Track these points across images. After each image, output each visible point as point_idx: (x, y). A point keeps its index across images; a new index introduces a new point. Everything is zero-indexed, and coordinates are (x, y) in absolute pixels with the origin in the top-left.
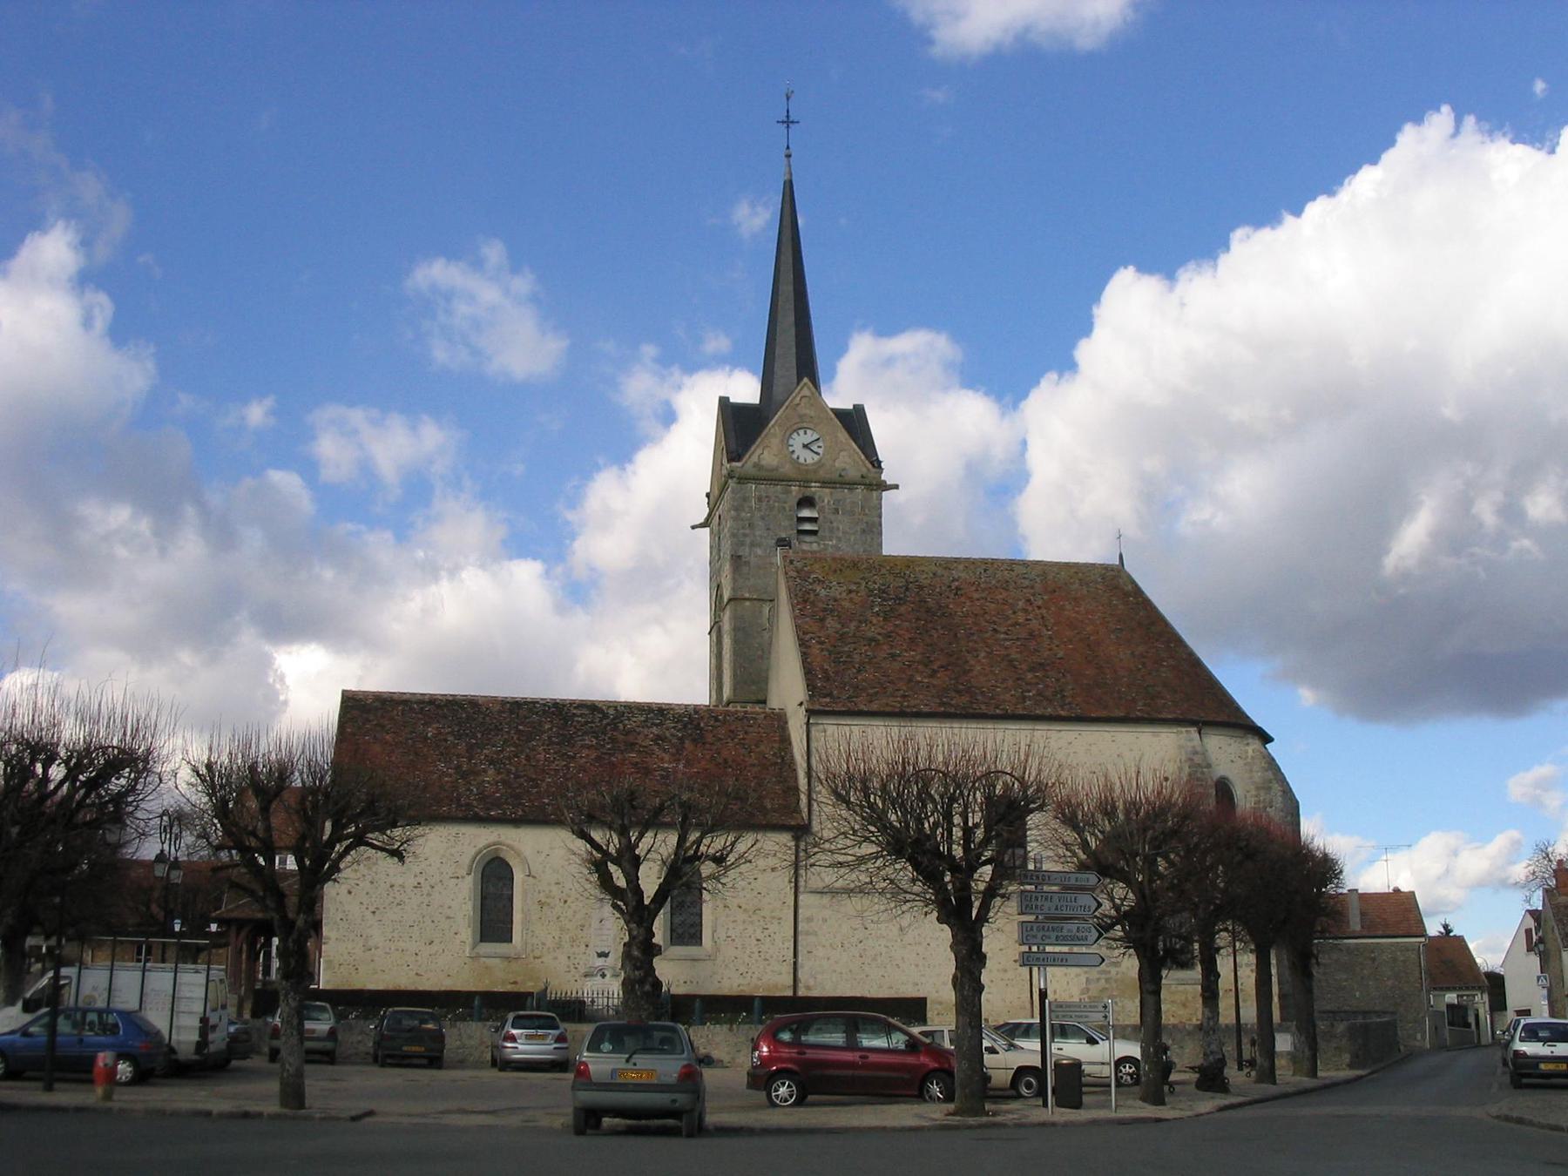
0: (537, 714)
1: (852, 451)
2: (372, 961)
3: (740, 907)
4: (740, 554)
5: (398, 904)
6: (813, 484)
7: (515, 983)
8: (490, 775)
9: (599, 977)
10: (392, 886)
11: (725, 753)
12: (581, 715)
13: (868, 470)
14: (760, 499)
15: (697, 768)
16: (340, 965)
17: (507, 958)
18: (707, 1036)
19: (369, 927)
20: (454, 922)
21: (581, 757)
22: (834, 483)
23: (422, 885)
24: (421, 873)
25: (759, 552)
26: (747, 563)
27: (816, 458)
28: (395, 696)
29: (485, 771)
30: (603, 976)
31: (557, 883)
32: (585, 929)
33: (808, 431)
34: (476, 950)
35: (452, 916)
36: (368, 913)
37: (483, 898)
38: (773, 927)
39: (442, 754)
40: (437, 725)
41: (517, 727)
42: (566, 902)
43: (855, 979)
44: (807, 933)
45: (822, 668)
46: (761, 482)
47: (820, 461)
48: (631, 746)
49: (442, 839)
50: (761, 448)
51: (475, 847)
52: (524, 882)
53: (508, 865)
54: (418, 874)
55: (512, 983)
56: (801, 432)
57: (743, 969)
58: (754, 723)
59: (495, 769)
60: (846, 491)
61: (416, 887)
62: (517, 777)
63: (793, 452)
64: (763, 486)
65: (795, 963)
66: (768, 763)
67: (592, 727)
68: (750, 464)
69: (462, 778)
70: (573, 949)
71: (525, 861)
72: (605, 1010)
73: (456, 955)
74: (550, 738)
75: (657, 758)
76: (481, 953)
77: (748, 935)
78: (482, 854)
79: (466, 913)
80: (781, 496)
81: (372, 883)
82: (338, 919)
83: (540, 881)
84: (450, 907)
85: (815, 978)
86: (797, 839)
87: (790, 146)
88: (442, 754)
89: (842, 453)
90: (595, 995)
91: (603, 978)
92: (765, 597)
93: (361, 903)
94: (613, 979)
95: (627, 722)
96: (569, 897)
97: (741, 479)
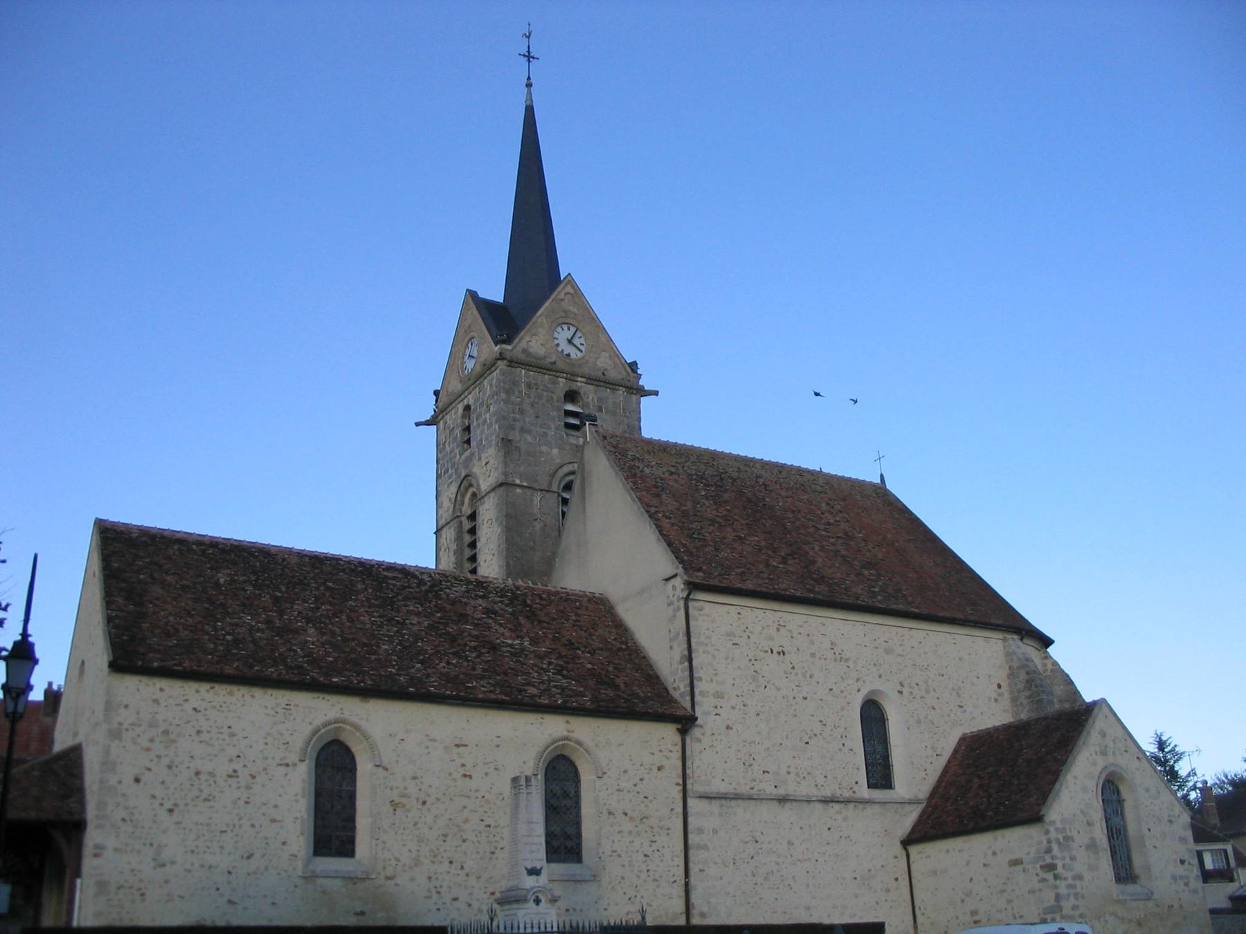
0: (343, 570)
1: (612, 354)
3: (626, 814)
5: (206, 800)
6: (579, 379)
7: (362, 913)
8: (311, 635)
12: (394, 578)
14: (529, 386)
16: (119, 888)
17: (351, 879)
24: (239, 756)
25: (529, 439)
26: (517, 448)
27: (579, 355)
28: (165, 533)
30: (537, 901)
31: (414, 778)
35: (279, 818)
36: (163, 814)
37: (318, 794)
40: (229, 571)
43: (749, 903)
44: (699, 847)
46: (531, 368)
47: (583, 358)
51: (311, 723)
54: (234, 758)
56: (565, 327)
57: (632, 893)
60: (608, 390)
61: (230, 776)
64: (531, 373)
65: (687, 884)
68: (519, 349)
71: (373, 747)
80: (549, 386)
81: (170, 767)
83: (393, 774)
85: (709, 902)
86: (683, 732)
87: (531, 77)
91: (538, 904)
96: (429, 796)
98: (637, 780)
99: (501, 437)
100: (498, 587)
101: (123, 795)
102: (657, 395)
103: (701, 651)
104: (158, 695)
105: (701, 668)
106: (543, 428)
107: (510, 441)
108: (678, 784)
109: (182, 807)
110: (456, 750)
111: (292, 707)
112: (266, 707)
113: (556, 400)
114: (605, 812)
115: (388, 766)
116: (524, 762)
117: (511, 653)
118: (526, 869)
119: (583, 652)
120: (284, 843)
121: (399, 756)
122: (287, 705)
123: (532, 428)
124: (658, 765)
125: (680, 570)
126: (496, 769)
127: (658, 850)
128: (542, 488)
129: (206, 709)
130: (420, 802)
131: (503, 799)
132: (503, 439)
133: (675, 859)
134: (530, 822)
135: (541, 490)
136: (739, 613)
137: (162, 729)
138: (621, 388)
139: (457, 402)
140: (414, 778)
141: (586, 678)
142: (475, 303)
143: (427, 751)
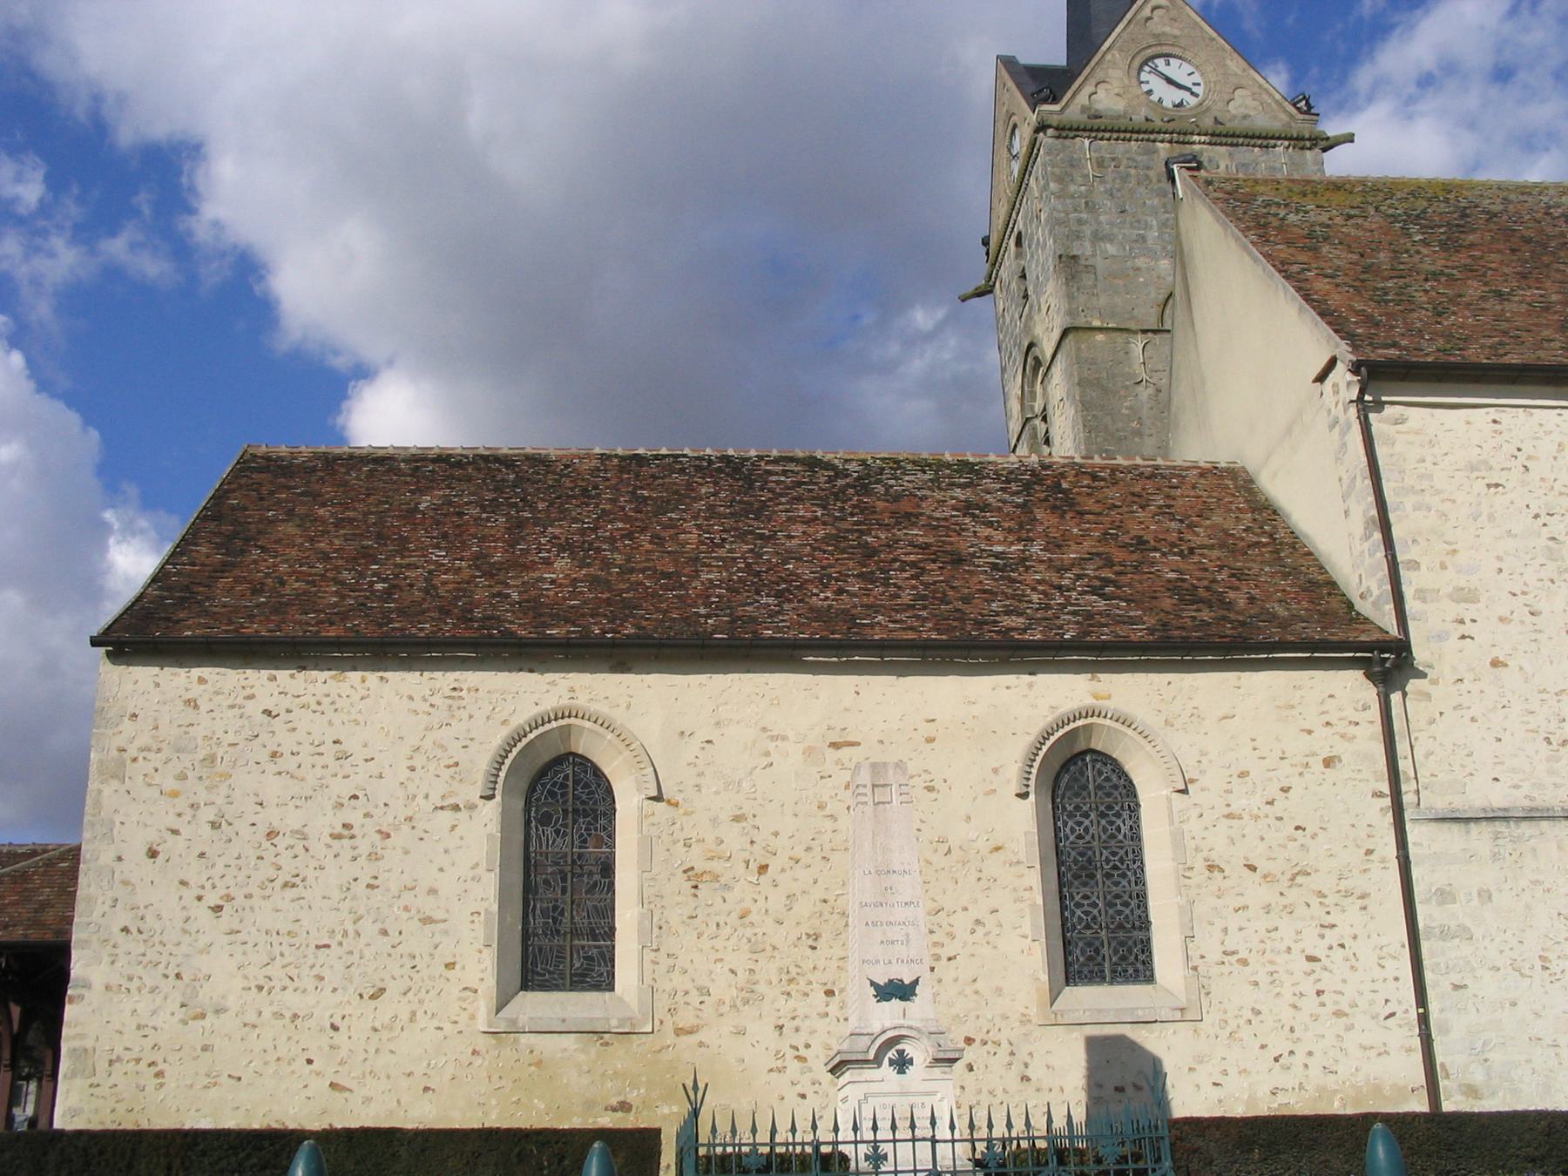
1: (1256, 89)
2: (205, 1048)
3: (1253, 868)
4: (1075, 252)
6: (1196, 138)
7: (624, 1107)
9: (886, 1070)
10: (271, 835)
11: (1135, 529)
13: (1291, 116)
14: (1100, 164)
19: (201, 952)
20: (446, 932)
21: (790, 537)
22: (1233, 136)
24: (355, 797)
26: (1090, 269)
27: (1193, 101)
29: (548, 562)
31: (737, 819)
32: (820, 944)
33: (1171, 60)
34: (507, 1012)
36: (202, 913)
37: (529, 865)
38: (1349, 919)
39: (445, 536)
42: (763, 869)
48: (910, 518)
49: (413, 705)
50: (1093, 81)
51: (505, 722)
52: (643, 816)
53: (598, 773)
55: (614, 1110)
57: (1279, 1045)
60: (1256, 150)
61: (338, 837)
63: (1150, 92)
65: (1424, 1020)
69: (488, 575)
70: (792, 1003)
73: (447, 1027)
74: (711, 508)
76: (523, 1021)
78: (525, 741)
79: (481, 907)
80: (1139, 158)
81: (215, 825)
82: (116, 929)
84: (433, 891)
88: (445, 536)
89: (1238, 92)
90: (884, 1133)
91: (901, 1071)
92: (1132, 325)
93: (183, 883)
94: (937, 1072)
95: (892, 482)
97: (1063, 129)
98: (1273, 792)
99: (1059, 253)
100: (1004, 469)
101: (126, 883)
102: (1352, 141)
103: (1408, 507)
104: (196, 691)
105: (1414, 541)
106: (1134, 228)
107: (1074, 257)
108: (1380, 795)
109: (240, 900)
110: (832, 754)
111: (463, 694)
112: (411, 698)
113: (1154, 180)
114: (1200, 865)
115: (679, 798)
116: (995, 771)
117: (994, 567)
118: (873, 984)
119: (1164, 554)
120: (450, 966)
121: (700, 775)
122: (455, 689)
123: (1115, 230)
124: (1326, 754)
125: (1343, 350)
126: (930, 789)
127: (1342, 946)
128: (1146, 327)
129: (289, 711)
130: (754, 866)
131: (949, 851)
132: (1060, 256)
133: (1388, 963)
134: (884, 872)
135: (1144, 332)
136: (1495, 422)
137: (201, 754)
138: (1279, 143)
139: (1007, 237)
140: (737, 819)
141: (1158, 595)
142: (1010, 73)
143: (765, 761)
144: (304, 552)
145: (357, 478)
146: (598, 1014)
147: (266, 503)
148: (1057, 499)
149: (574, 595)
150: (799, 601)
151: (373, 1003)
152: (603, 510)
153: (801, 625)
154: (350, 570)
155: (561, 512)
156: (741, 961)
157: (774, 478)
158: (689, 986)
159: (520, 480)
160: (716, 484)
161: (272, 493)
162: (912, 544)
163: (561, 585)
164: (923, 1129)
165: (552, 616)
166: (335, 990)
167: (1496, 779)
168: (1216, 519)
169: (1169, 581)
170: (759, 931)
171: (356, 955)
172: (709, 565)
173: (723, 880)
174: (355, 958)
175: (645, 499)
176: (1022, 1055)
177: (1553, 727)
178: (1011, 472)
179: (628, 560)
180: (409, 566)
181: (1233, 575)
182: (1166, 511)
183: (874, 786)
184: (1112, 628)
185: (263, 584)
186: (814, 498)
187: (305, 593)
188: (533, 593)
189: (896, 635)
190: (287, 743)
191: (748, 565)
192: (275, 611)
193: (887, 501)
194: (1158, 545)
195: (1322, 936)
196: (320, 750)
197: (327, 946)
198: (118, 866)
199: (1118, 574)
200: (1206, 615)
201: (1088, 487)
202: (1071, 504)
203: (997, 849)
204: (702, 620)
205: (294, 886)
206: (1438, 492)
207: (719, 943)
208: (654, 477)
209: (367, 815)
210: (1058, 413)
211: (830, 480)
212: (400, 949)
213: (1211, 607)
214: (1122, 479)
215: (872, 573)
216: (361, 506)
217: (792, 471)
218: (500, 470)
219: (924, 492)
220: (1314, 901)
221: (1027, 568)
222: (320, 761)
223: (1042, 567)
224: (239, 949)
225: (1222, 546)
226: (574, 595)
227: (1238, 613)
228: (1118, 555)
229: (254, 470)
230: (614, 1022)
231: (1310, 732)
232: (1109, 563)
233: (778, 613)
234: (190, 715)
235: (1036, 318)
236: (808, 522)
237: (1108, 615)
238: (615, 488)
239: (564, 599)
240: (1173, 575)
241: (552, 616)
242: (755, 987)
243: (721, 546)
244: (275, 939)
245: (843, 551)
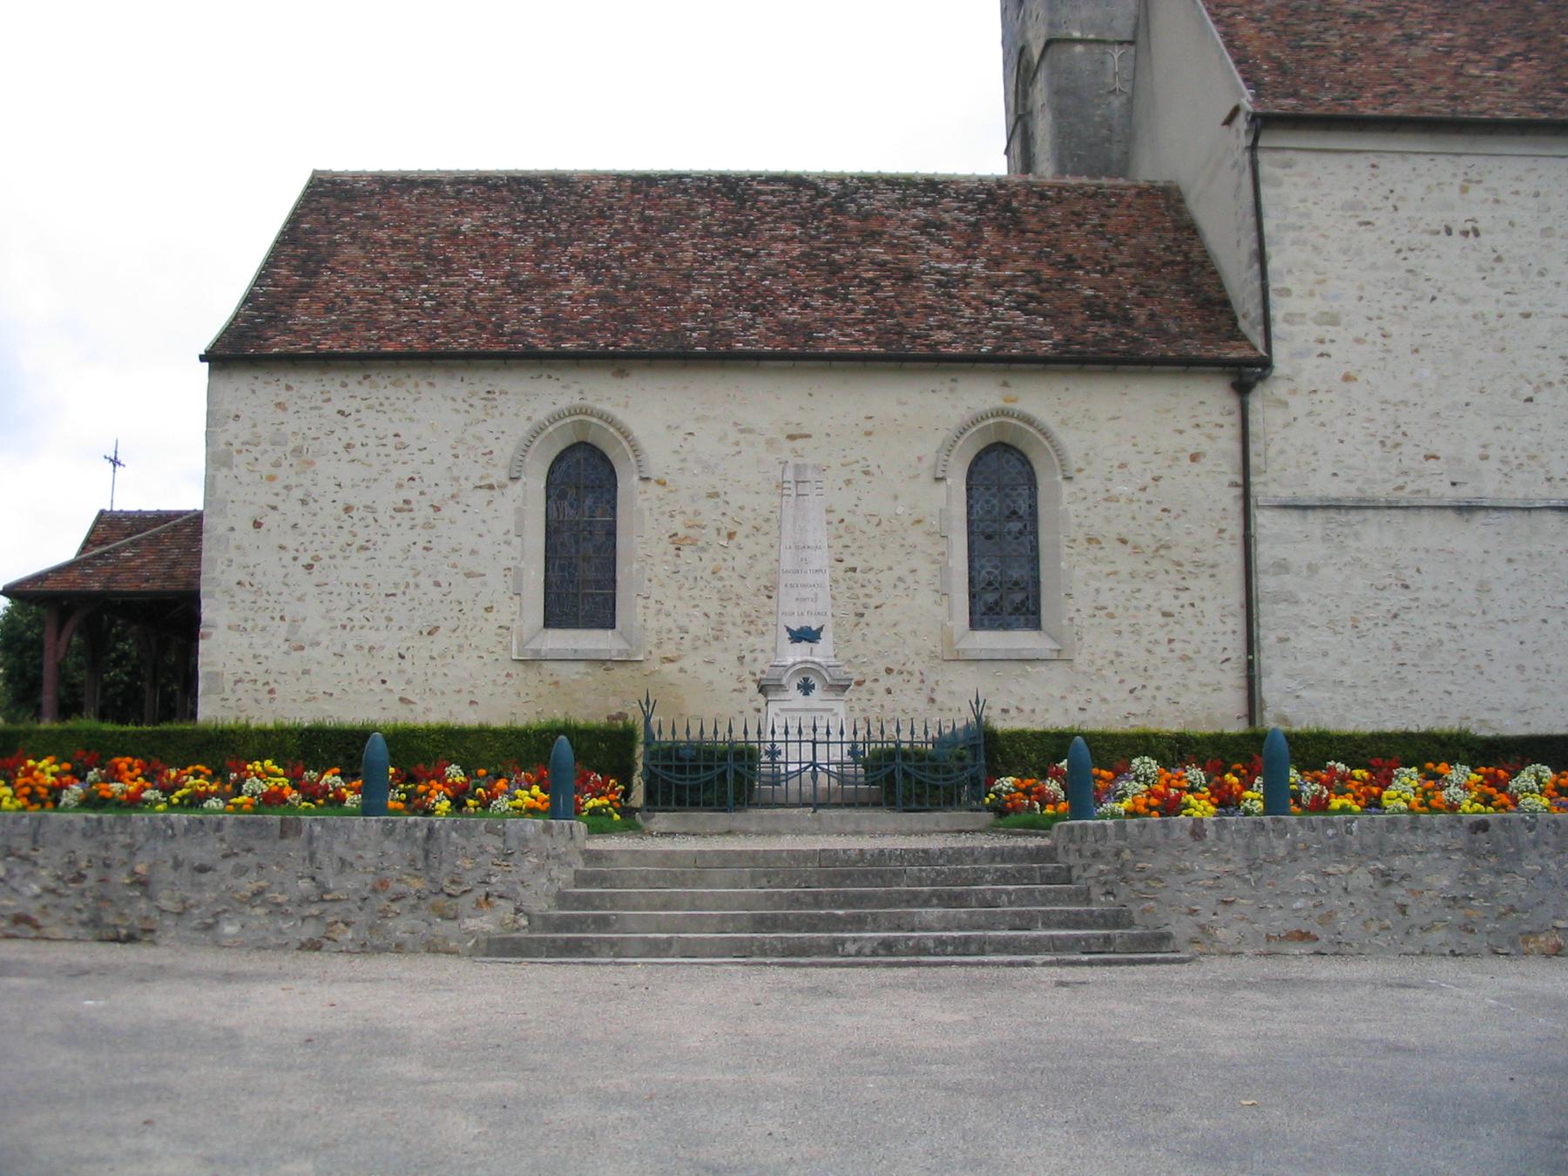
3: (1124, 542)
5: (363, 548)
10: (348, 509)
11: (1069, 248)
15: (1012, 270)
18: (1118, 854)
21: (770, 255)
23: (414, 505)
24: (412, 479)
29: (566, 280)
36: (297, 570)
39: (482, 256)
41: (642, 213)
42: (731, 536)
44: (1277, 598)
45: (1269, 58)
48: (873, 237)
51: (529, 419)
57: (1134, 681)
58: (1119, 202)
59: (588, 277)
62: (631, 287)
66: (1158, 263)
67: (793, 210)
69: (516, 292)
72: (806, 775)
74: (706, 227)
75: (928, 254)
77: (1144, 604)
81: (304, 502)
84: (473, 552)
88: (482, 256)
90: (779, 736)
91: (806, 694)
92: (1109, 37)
95: (864, 201)
100: (964, 188)
101: (238, 548)
109: (326, 561)
114: (1081, 538)
117: (939, 284)
120: (488, 609)
121: (684, 460)
124: (1192, 450)
126: (866, 473)
127: (1193, 605)
129: (358, 411)
130: (724, 533)
134: (801, 547)
135: (1121, 43)
136: (1373, 166)
144: (366, 272)
145: (410, 201)
146: (602, 646)
147: (334, 227)
148: (1004, 218)
149: (587, 310)
150: (772, 315)
151: (431, 638)
152: (615, 230)
153: (767, 338)
154: (404, 289)
155: (579, 233)
156: (713, 607)
157: (763, 198)
158: (672, 625)
159: (546, 201)
160: (712, 203)
161: (339, 216)
162: (872, 262)
163: (576, 302)
164: (808, 734)
165: (566, 330)
166: (401, 628)
167: (1335, 474)
168: (1142, 238)
169: (1086, 298)
170: (727, 583)
171: (416, 602)
172: (701, 282)
173: (700, 544)
174: (416, 604)
175: (651, 218)
176: (930, 682)
177: (1388, 432)
178: (970, 191)
179: (633, 278)
180: (452, 284)
181: (1141, 293)
182: (1099, 232)
183: (797, 482)
184: (1024, 342)
185: (334, 303)
186: (795, 217)
187: (370, 311)
188: (553, 308)
189: (842, 349)
190: (357, 436)
191: (732, 281)
192: (345, 328)
193: (858, 220)
194: (1084, 264)
195: (1176, 597)
196: (384, 442)
197: (394, 595)
198: (231, 535)
199: (1043, 290)
200: (1107, 331)
201: (1035, 206)
202: (1017, 221)
203: (919, 522)
204: (688, 333)
205: (367, 549)
206: (1316, 228)
207: (695, 592)
208: (660, 197)
209: (422, 493)
210: (1040, 116)
211: (812, 199)
212: (449, 598)
213: (1114, 322)
214: (1067, 199)
215: (835, 289)
216: (413, 229)
217: (780, 191)
218: (529, 192)
219: (892, 211)
220: (1172, 569)
221: (967, 285)
222: (382, 450)
223: (979, 284)
224: (325, 597)
225: (1139, 264)
226: (587, 310)
227: (1136, 330)
228: (1047, 273)
229: (322, 195)
230: (614, 653)
231: (1181, 432)
232: (1038, 281)
233: (752, 327)
234: (281, 416)
235: (1029, 24)
236: (787, 240)
237: (1024, 330)
238: (627, 209)
239: (579, 314)
240: (1090, 292)
241: (566, 330)
242: (724, 627)
243: (712, 263)
244: (355, 590)
245: (813, 268)
